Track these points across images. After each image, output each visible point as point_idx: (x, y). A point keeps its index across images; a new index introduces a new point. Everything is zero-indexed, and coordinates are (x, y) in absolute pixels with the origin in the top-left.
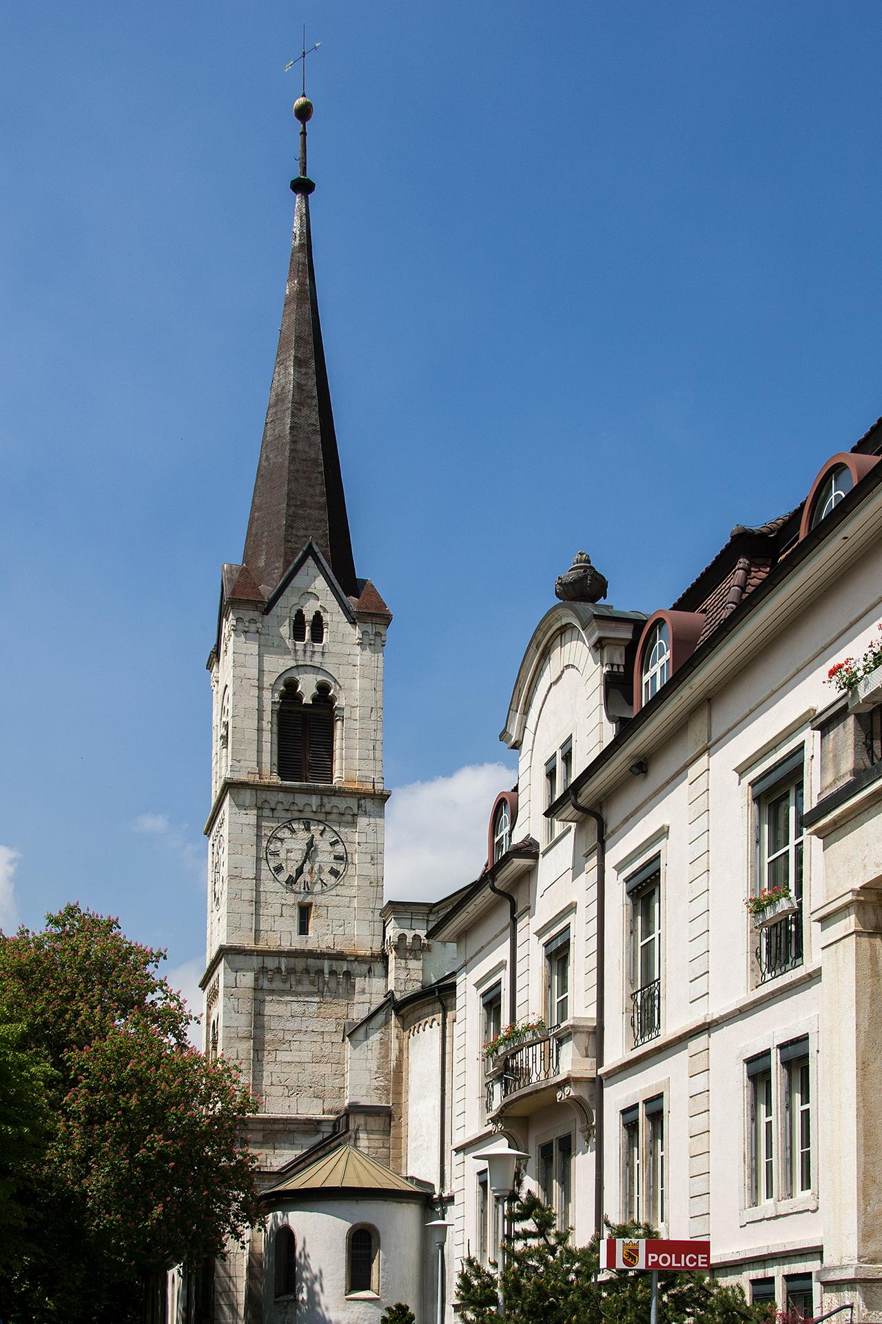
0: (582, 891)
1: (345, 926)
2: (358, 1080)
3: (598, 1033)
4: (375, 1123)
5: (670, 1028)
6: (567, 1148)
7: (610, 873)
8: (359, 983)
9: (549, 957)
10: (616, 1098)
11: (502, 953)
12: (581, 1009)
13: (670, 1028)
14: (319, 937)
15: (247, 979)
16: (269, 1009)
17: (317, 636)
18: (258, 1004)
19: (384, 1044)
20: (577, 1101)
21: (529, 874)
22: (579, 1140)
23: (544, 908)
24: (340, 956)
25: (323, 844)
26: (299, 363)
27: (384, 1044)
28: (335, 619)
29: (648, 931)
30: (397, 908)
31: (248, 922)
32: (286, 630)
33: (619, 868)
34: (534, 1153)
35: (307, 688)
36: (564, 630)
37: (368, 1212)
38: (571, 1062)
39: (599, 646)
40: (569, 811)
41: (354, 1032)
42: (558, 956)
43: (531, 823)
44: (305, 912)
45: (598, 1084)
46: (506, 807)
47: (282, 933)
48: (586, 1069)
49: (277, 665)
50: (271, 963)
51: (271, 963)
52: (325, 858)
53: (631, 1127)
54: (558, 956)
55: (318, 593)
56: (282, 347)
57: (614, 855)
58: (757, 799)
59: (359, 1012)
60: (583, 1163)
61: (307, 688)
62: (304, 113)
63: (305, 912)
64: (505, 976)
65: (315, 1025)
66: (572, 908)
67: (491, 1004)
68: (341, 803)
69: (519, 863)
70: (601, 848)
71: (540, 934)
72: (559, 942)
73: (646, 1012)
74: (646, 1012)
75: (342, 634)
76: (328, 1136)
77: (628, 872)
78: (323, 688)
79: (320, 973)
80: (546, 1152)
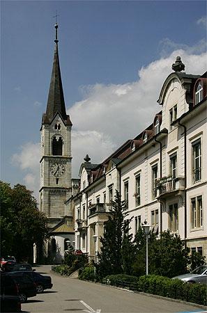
0: (115, 182)
1: (65, 183)
2: (67, 213)
3: (185, 179)
4: (70, 219)
5: (142, 205)
6: (176, 207)
7: (187, 141)
8: (67, 193)
9: (153, 169)
10: (190, 195)
11: (158, 156)
12: (180, 174)
13: (142, 205)
14: (59, 185)
15: (47, 193)
16: (51, 198)
17: (59, 128)
18: (49, 197)
19: (71, 205)
20: (180, 196)
21: (165, 137)
22: (179, 204)
23: (170, 147)
24: (64, 188)
25: (60, 167)
26: (56, 76)
27: (71, 205)
28: (62, 125)
29: (174, 167)
30: (73, 180)
31: (47, 182)
32: (54, 128)
33: (190, 140)
34: (167, 207)
35: (57, 138)
36: (173, 79)
37: (67, 236)
38: (178, 186)
39: (184, 85)
40: (177, 124)
41: (66, 203)
42: (173, 159)
43: (166, 124)
44: (57, 180)
45: (185, 191)
46: (159, 118)
47: (54, 184)
48: (182, 188)
49: (52, 134)
50: (51, 190)
51: (51, 190)
52: (61, 170)
53: (193, 203)
54: (173, 159)
55: (60, 121)
56: (53, 72)
57: (188, 137)
58: (193, 146)
59: (67, 199)
60: (181, 210)
61: (57, 138)
62: (57, 27)
63: (57, 180)
64: (159, 162)
65: (59, 201)
66: (177, 148)
67: (155, 169)
68: (64, 160)
69: (163, 134)
70: (185, 134)
71: (169, 153)
72: (197, 144)
73: (138, 201)
74: (138, 201)
75: (63, 128)
76: (62, 222)
77: (192, 141)
78: (60, 138)
79: (60, 191)
80: (171, 207)
